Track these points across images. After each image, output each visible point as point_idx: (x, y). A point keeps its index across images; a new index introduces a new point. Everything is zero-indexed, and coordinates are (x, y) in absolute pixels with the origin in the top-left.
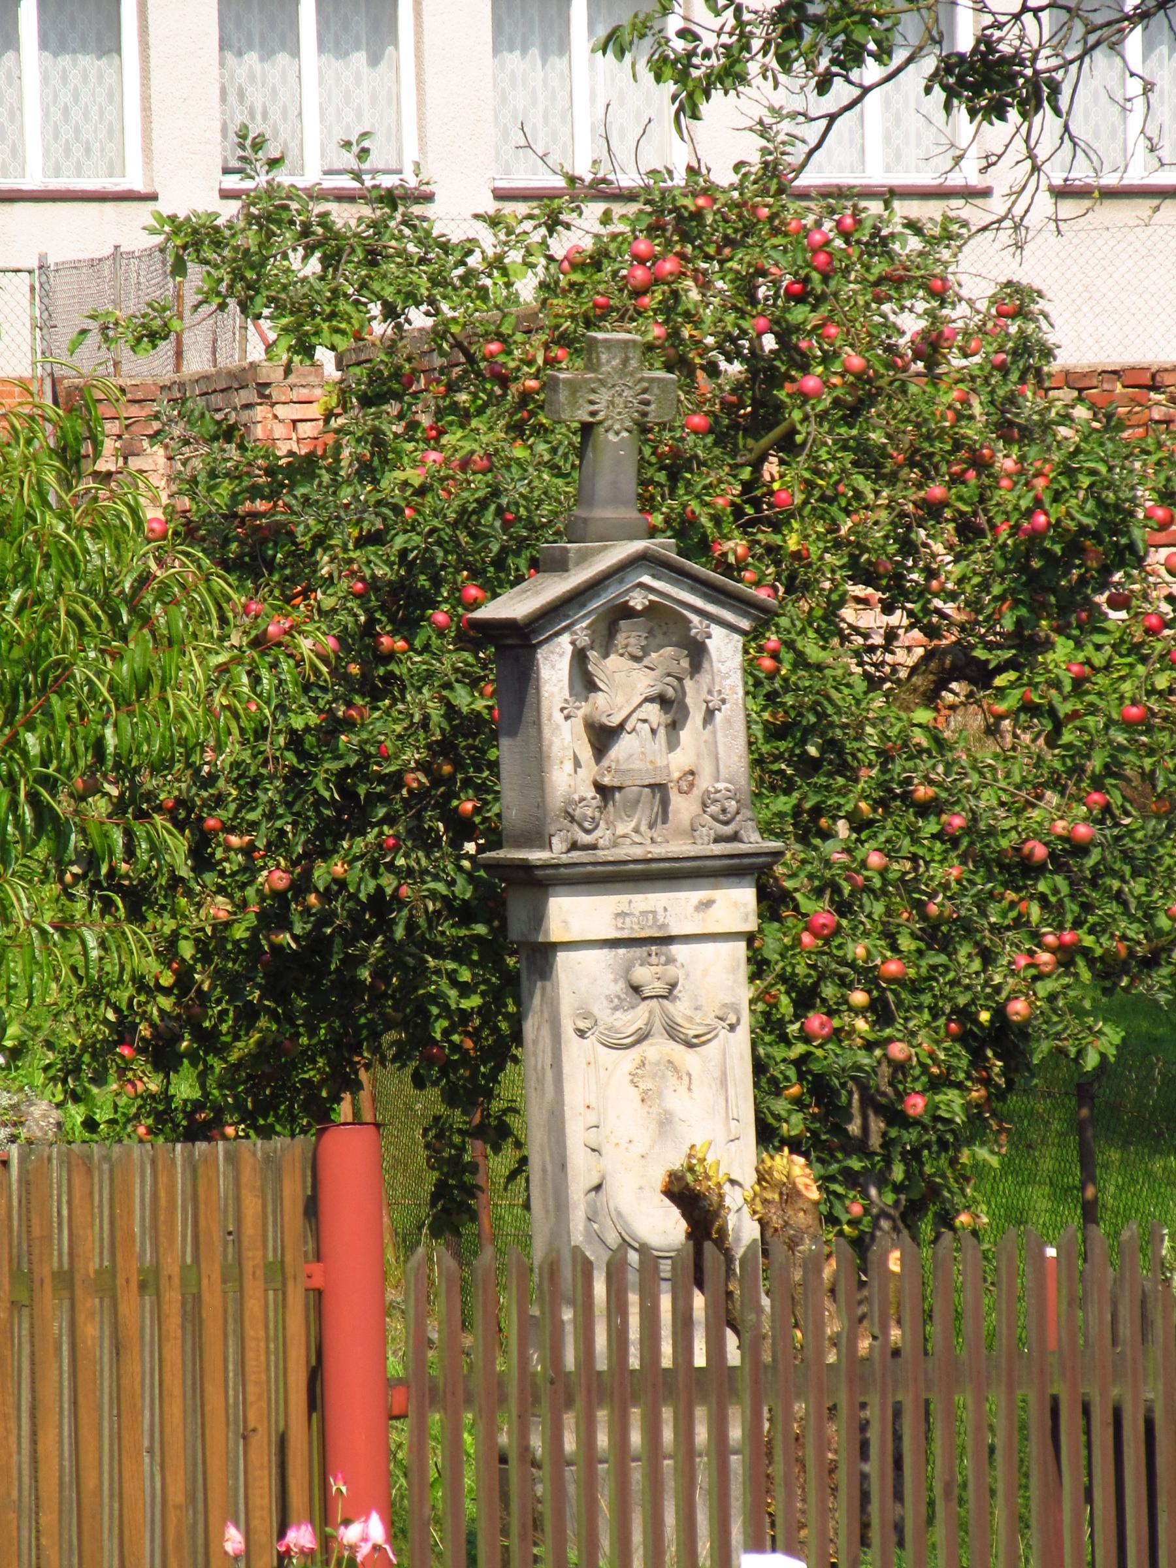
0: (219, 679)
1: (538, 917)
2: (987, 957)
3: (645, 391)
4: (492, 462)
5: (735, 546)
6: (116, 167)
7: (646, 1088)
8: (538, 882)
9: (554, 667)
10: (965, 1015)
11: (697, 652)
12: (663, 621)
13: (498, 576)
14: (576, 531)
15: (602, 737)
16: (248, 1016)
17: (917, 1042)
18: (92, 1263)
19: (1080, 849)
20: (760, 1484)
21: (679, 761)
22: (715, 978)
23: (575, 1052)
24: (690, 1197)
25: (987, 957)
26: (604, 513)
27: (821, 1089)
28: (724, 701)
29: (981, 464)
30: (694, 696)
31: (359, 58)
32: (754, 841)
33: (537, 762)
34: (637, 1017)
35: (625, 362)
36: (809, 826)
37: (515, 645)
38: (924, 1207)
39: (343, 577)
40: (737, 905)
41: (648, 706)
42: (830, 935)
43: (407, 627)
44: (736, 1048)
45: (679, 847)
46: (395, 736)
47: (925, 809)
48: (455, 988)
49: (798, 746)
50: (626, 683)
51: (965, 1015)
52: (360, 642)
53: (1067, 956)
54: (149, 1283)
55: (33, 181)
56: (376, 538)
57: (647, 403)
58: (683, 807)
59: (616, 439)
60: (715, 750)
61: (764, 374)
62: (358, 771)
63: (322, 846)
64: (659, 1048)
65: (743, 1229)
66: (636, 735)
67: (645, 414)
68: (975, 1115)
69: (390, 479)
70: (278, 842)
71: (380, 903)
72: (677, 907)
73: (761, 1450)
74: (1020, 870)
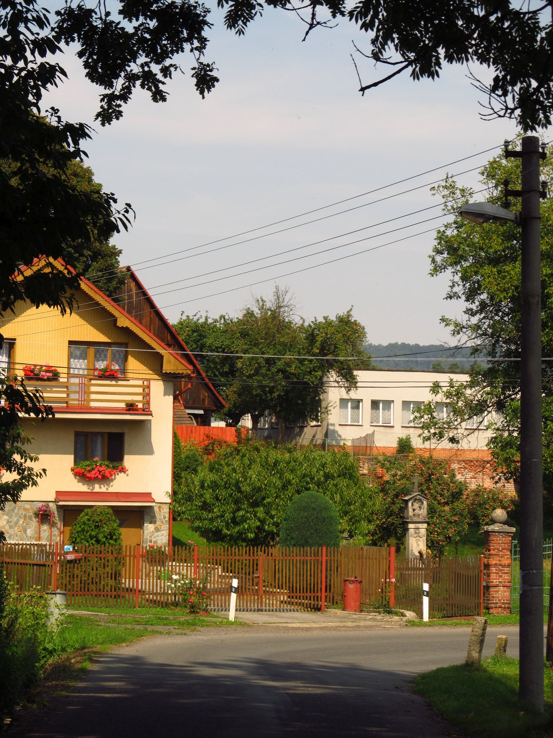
0: (379, 502)
1: (408, 526)
2: (448, 530)
4: (405, 484)
5: (426, 492)
6: (358, 422)
7: (417, 543)
8: (408, 523)
9: (410, 504)
10: (445, 535)
11: (423, 503)
12: (420, 500)
13: (406, 495)
14: (412, 491)
15: (414, 510)
16: (380, 532)
17: (441, 538)
18: (371, 557)
19: (457, 521)
20: (425, 577)
21: (421, 512)
22: (423, 532)
23: (411, 538)
24: (420, 553)
25: (448, 530)
26: (415, 490)
27: (432, 541)
29: (449, 485)
30: (422, 507)
31: (387, 411)
32: (427, 520)
33: (408, 512)
34: (416, 535)
36: (432, 517)
37: (406, 502)
38: (441, 552)
39: (392, 493)
40: (425, 525)
42: (433, 528)
43: (397, 498)
44: (425, 538)
45: (420, 520)
46: (395, 508)
47: (443, 517)
48: (399, 531)
49: (432, 511)
50: (416, 505)
51: (445, 535)
52: (393, 499)
53: (455, 530)
54: (376, 559)
55: (349, 423)
56: (394, 490)
58: (421, 517)
59: (416, 484)
60: (424, 512)
61: (430, 475)
62: (392, 511)
63: (388, 518)
64: (418, 538)
65: (425, 557)
66: (417, 510)
68: (446, 544)
69: (396, 485)
70: (384, 517)
71: (393, 523)
72: (420, 525)
73: (425, 574)
74: (451, 523)
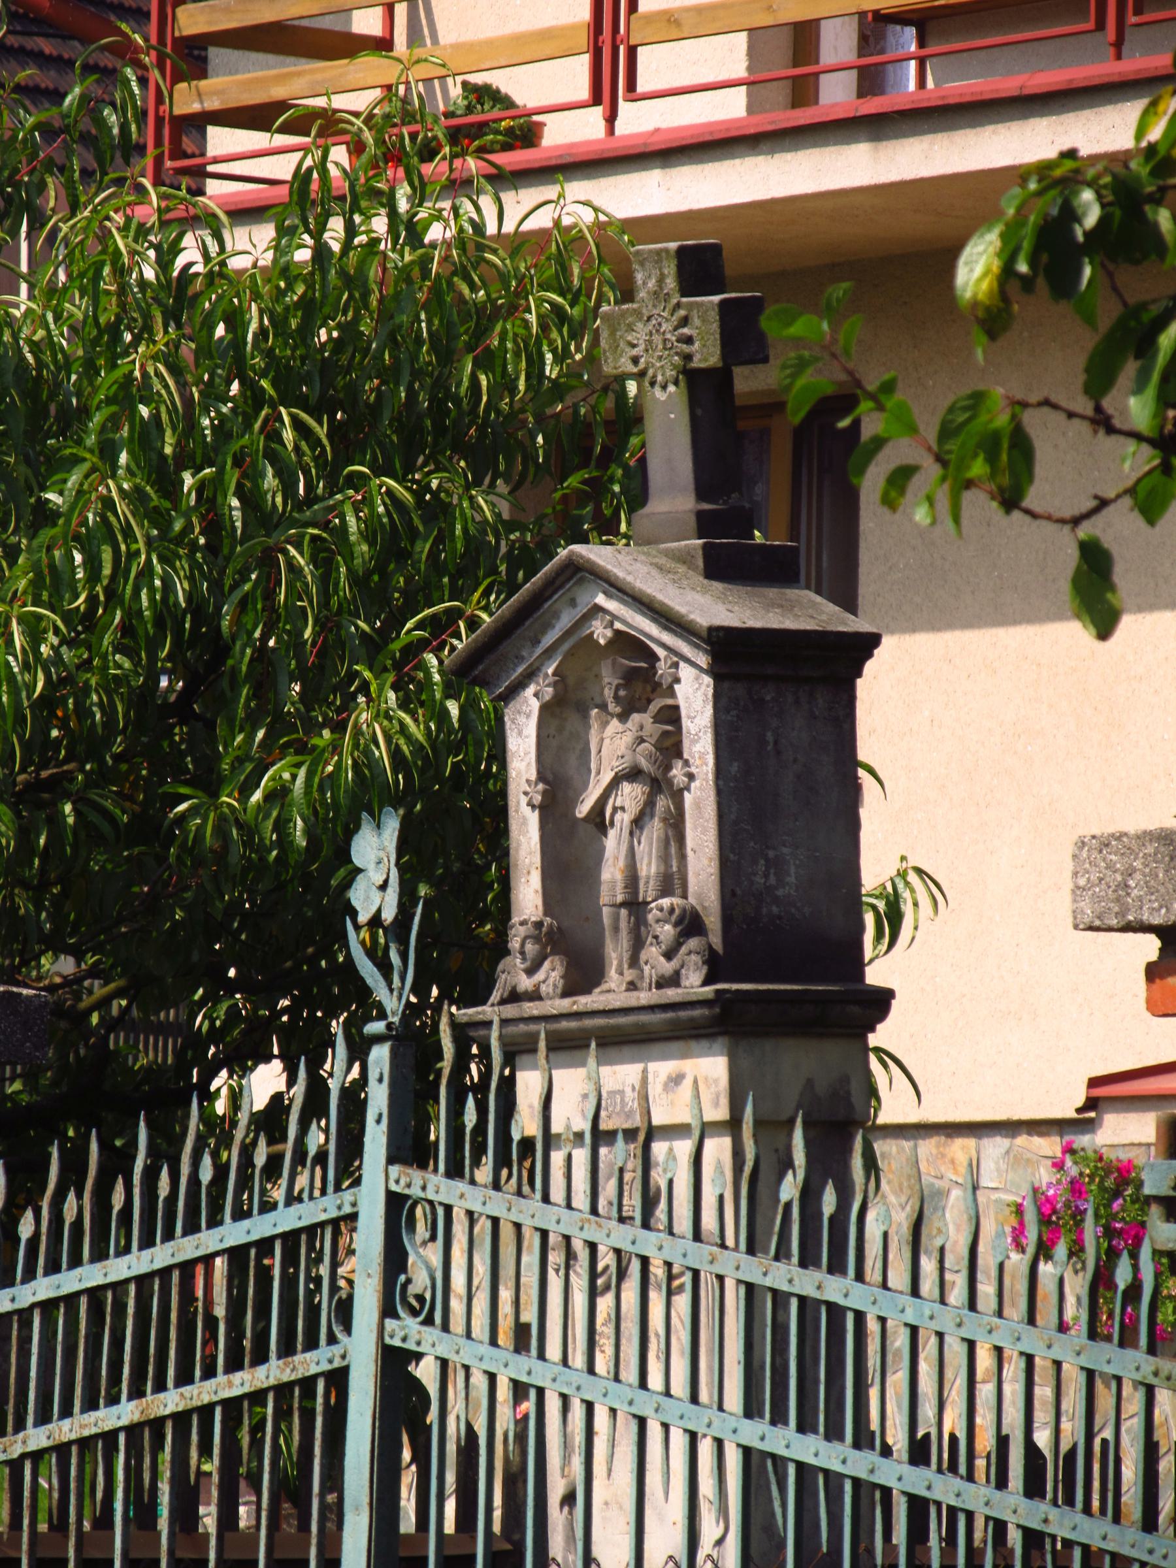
3: (685, 321)
28: (691, 777)
35: (661, 280)
41: (626, 787)
57: (689, 340)
67: (688, 357)
